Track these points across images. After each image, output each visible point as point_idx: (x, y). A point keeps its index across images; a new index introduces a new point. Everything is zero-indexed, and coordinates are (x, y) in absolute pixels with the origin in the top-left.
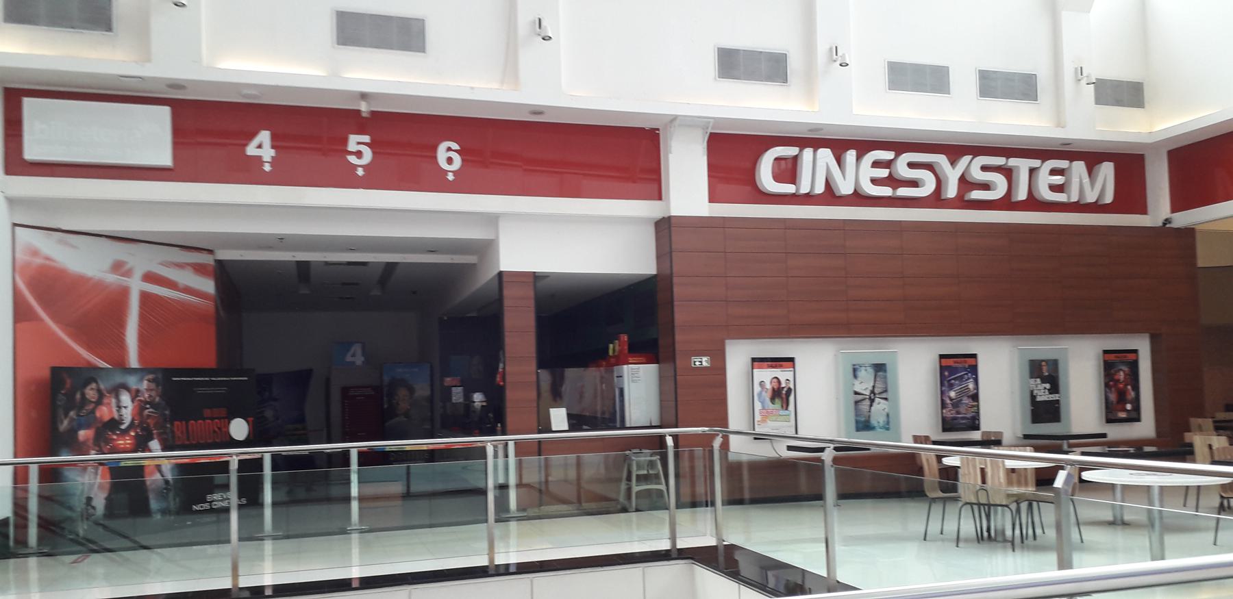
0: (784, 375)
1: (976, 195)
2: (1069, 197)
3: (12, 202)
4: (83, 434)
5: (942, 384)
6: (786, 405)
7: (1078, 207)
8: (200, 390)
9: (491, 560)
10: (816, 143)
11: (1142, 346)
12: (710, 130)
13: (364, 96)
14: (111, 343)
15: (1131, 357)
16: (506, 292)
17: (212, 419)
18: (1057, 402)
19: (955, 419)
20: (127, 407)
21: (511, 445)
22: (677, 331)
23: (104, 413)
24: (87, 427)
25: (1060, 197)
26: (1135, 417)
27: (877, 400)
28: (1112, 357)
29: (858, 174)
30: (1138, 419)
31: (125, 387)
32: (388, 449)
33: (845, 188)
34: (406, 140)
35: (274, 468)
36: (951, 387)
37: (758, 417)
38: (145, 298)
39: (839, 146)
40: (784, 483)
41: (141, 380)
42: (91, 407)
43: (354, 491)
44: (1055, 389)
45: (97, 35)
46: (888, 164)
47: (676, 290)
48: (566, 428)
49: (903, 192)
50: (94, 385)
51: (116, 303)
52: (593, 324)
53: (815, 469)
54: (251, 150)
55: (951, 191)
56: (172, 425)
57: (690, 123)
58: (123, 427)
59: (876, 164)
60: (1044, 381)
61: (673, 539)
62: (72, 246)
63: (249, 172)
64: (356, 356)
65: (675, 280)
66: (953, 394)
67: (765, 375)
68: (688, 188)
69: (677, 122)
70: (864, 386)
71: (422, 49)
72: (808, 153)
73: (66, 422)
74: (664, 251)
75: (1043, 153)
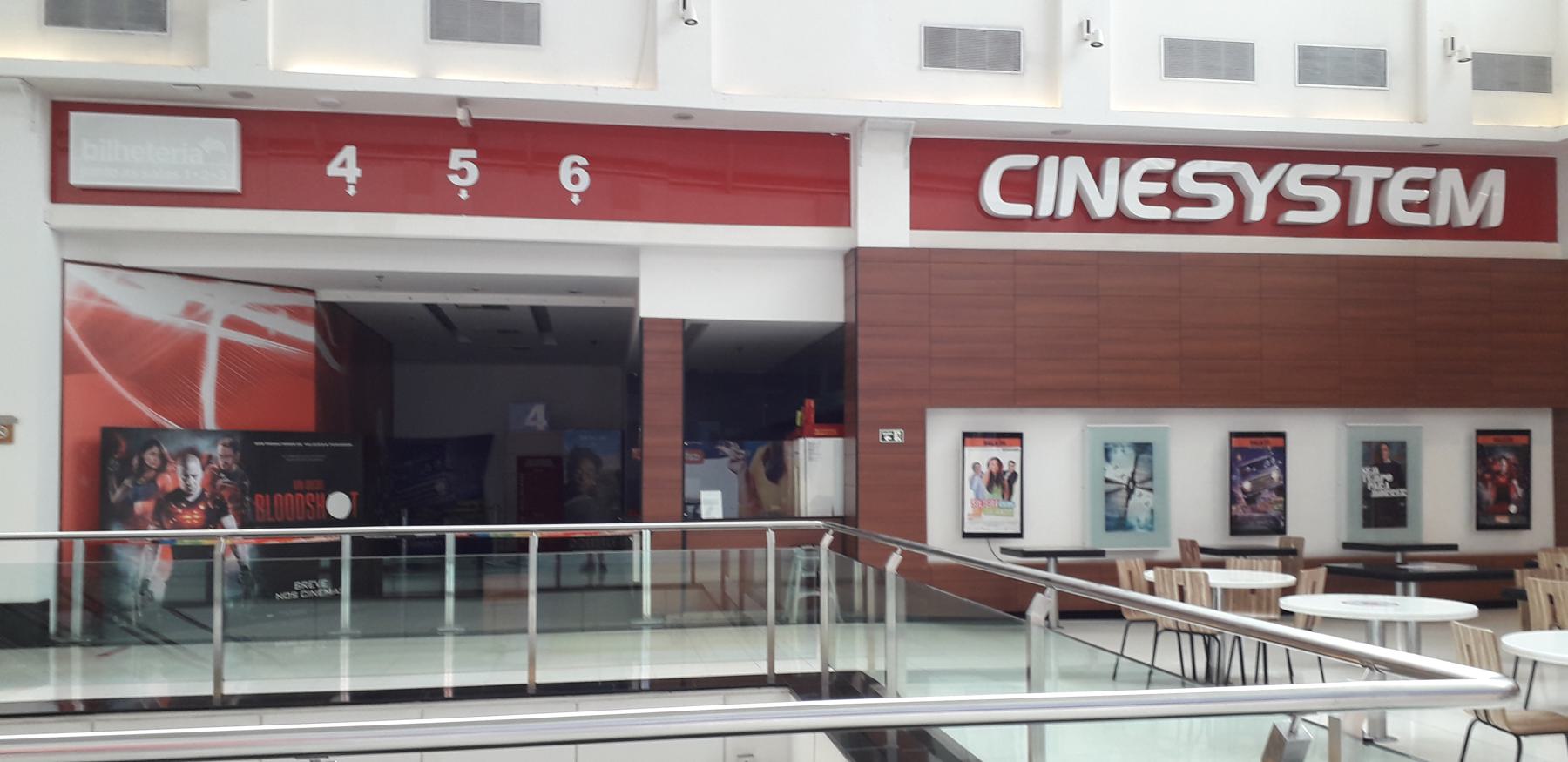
0: (1007, 455)
1: (1292, 216)
2: (1433, 219)
3: (61, 234)
4: (139, 506)
5: (1232, 472)
6: (1008, 494)
7: (1450, 232)
8: (291, 458)
9: (871, 665)
10: (1063, 150)
11: (1540, 428)
12: (912, 135)
13: (462, 102)
14: (183, 402)
15: (1521, 440)
16: (646, 345)
17: (304, 492)
18: (1403, 499)
19: (1244, 518)
20: (196, 477)
21: (647, 535)
22: (860, 398)
23: (167, 481)
24: (146, 498)
25: (1422, 219)
26: (1522, 522)
27: (1137, 491)
28: (1490, 440)
29: (1126, 189)
30: (1526, 526)
31: (194, 452)
32: (492, 535)
33: (1103, 208)
34: (521, 154)
35: (354, 552)
36: (1245, 476)
37: (968, 509)
38: (226, 347)
39: (1095, 153)
40: (985, 600)
41: (215, 444)
42: (150, 474)
43: (450, 585)
44: (1400, 481)
45: (150, 36)
46: (1168, 177)
47: (861, 343)
48: (720, 516)
49: (1185, 213)
50: (155, 449)
51: (191, 351)
52: (764, 390)
53: (365, 589)
54: (333, 170)
55: (1257, 211)
56: (253, 497)
57: (885, 126)
58: (190, 499)
59: (1149, 176)
60: (1384, 469)
61: (218, 680)
62: (138, 286)
63: (332, 198)
64: (537, 417)
65: (860, 330)
66: (1247, 485)
67: (980, 455)
68: (883, 210)
69: (867, 125)
70: (1120, 472)
71: (534, 40)
72: (1052, 162)
73: (119, 492)
74: (854, 295)
75: (1397, 160)
